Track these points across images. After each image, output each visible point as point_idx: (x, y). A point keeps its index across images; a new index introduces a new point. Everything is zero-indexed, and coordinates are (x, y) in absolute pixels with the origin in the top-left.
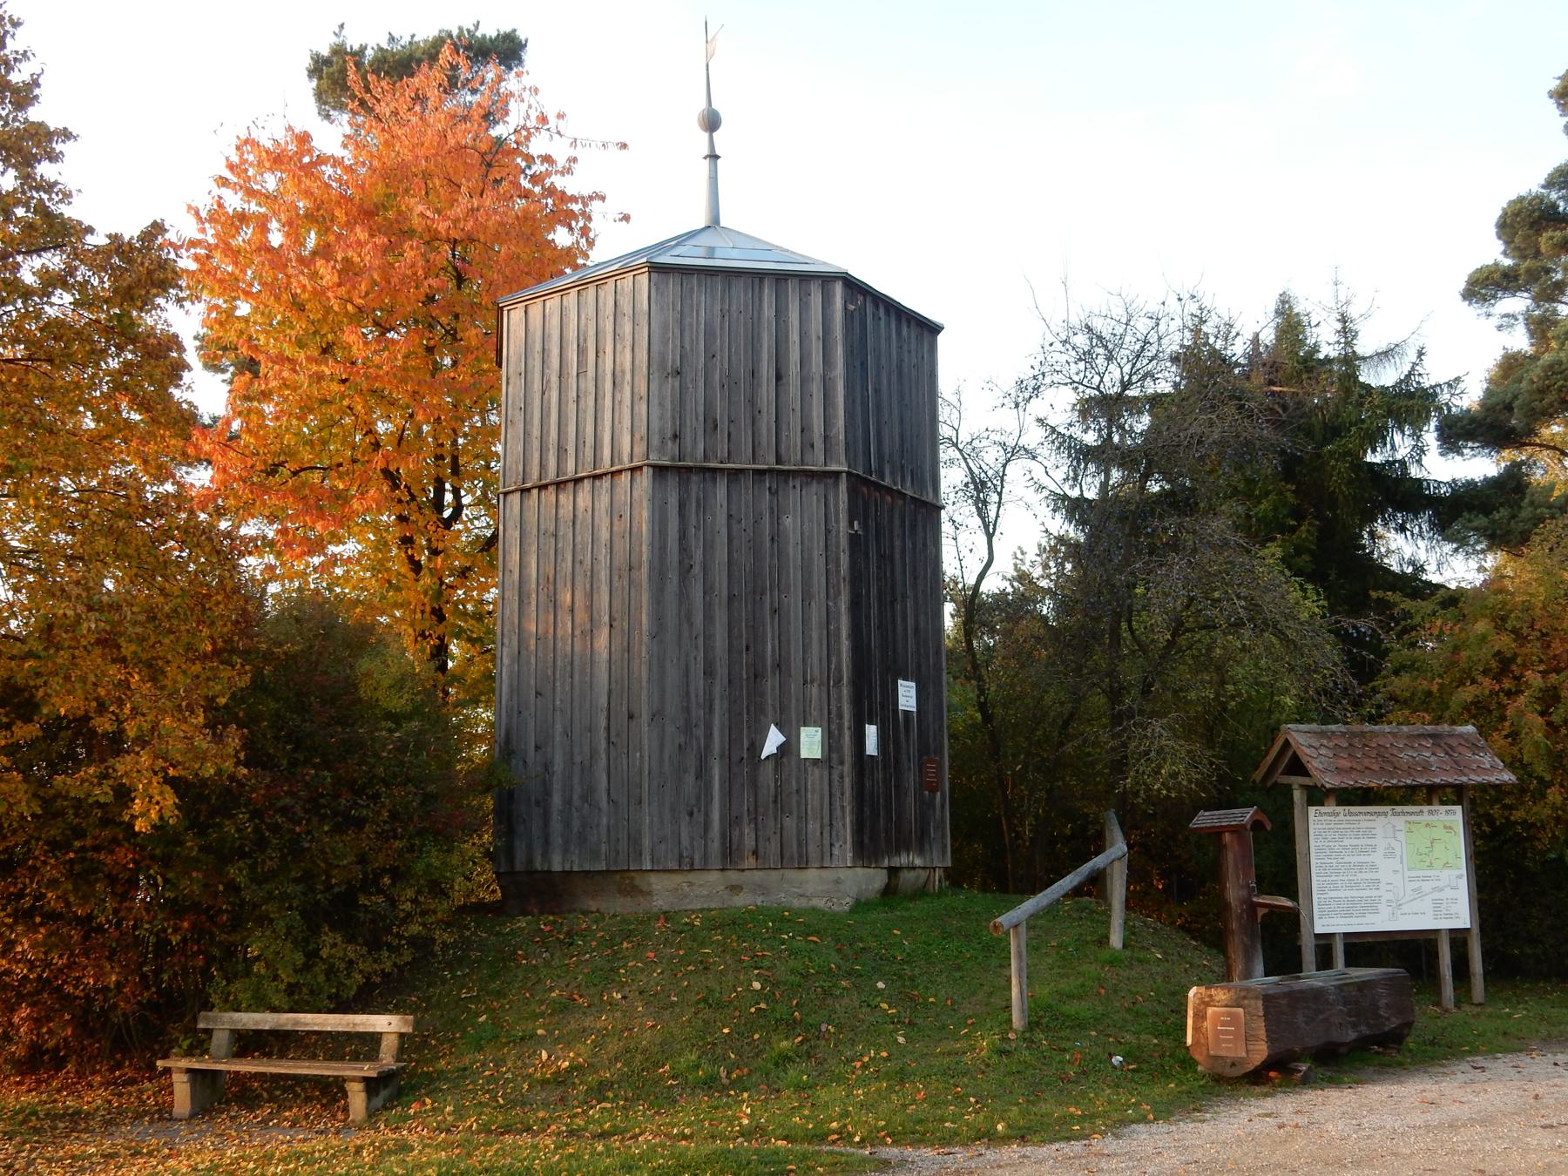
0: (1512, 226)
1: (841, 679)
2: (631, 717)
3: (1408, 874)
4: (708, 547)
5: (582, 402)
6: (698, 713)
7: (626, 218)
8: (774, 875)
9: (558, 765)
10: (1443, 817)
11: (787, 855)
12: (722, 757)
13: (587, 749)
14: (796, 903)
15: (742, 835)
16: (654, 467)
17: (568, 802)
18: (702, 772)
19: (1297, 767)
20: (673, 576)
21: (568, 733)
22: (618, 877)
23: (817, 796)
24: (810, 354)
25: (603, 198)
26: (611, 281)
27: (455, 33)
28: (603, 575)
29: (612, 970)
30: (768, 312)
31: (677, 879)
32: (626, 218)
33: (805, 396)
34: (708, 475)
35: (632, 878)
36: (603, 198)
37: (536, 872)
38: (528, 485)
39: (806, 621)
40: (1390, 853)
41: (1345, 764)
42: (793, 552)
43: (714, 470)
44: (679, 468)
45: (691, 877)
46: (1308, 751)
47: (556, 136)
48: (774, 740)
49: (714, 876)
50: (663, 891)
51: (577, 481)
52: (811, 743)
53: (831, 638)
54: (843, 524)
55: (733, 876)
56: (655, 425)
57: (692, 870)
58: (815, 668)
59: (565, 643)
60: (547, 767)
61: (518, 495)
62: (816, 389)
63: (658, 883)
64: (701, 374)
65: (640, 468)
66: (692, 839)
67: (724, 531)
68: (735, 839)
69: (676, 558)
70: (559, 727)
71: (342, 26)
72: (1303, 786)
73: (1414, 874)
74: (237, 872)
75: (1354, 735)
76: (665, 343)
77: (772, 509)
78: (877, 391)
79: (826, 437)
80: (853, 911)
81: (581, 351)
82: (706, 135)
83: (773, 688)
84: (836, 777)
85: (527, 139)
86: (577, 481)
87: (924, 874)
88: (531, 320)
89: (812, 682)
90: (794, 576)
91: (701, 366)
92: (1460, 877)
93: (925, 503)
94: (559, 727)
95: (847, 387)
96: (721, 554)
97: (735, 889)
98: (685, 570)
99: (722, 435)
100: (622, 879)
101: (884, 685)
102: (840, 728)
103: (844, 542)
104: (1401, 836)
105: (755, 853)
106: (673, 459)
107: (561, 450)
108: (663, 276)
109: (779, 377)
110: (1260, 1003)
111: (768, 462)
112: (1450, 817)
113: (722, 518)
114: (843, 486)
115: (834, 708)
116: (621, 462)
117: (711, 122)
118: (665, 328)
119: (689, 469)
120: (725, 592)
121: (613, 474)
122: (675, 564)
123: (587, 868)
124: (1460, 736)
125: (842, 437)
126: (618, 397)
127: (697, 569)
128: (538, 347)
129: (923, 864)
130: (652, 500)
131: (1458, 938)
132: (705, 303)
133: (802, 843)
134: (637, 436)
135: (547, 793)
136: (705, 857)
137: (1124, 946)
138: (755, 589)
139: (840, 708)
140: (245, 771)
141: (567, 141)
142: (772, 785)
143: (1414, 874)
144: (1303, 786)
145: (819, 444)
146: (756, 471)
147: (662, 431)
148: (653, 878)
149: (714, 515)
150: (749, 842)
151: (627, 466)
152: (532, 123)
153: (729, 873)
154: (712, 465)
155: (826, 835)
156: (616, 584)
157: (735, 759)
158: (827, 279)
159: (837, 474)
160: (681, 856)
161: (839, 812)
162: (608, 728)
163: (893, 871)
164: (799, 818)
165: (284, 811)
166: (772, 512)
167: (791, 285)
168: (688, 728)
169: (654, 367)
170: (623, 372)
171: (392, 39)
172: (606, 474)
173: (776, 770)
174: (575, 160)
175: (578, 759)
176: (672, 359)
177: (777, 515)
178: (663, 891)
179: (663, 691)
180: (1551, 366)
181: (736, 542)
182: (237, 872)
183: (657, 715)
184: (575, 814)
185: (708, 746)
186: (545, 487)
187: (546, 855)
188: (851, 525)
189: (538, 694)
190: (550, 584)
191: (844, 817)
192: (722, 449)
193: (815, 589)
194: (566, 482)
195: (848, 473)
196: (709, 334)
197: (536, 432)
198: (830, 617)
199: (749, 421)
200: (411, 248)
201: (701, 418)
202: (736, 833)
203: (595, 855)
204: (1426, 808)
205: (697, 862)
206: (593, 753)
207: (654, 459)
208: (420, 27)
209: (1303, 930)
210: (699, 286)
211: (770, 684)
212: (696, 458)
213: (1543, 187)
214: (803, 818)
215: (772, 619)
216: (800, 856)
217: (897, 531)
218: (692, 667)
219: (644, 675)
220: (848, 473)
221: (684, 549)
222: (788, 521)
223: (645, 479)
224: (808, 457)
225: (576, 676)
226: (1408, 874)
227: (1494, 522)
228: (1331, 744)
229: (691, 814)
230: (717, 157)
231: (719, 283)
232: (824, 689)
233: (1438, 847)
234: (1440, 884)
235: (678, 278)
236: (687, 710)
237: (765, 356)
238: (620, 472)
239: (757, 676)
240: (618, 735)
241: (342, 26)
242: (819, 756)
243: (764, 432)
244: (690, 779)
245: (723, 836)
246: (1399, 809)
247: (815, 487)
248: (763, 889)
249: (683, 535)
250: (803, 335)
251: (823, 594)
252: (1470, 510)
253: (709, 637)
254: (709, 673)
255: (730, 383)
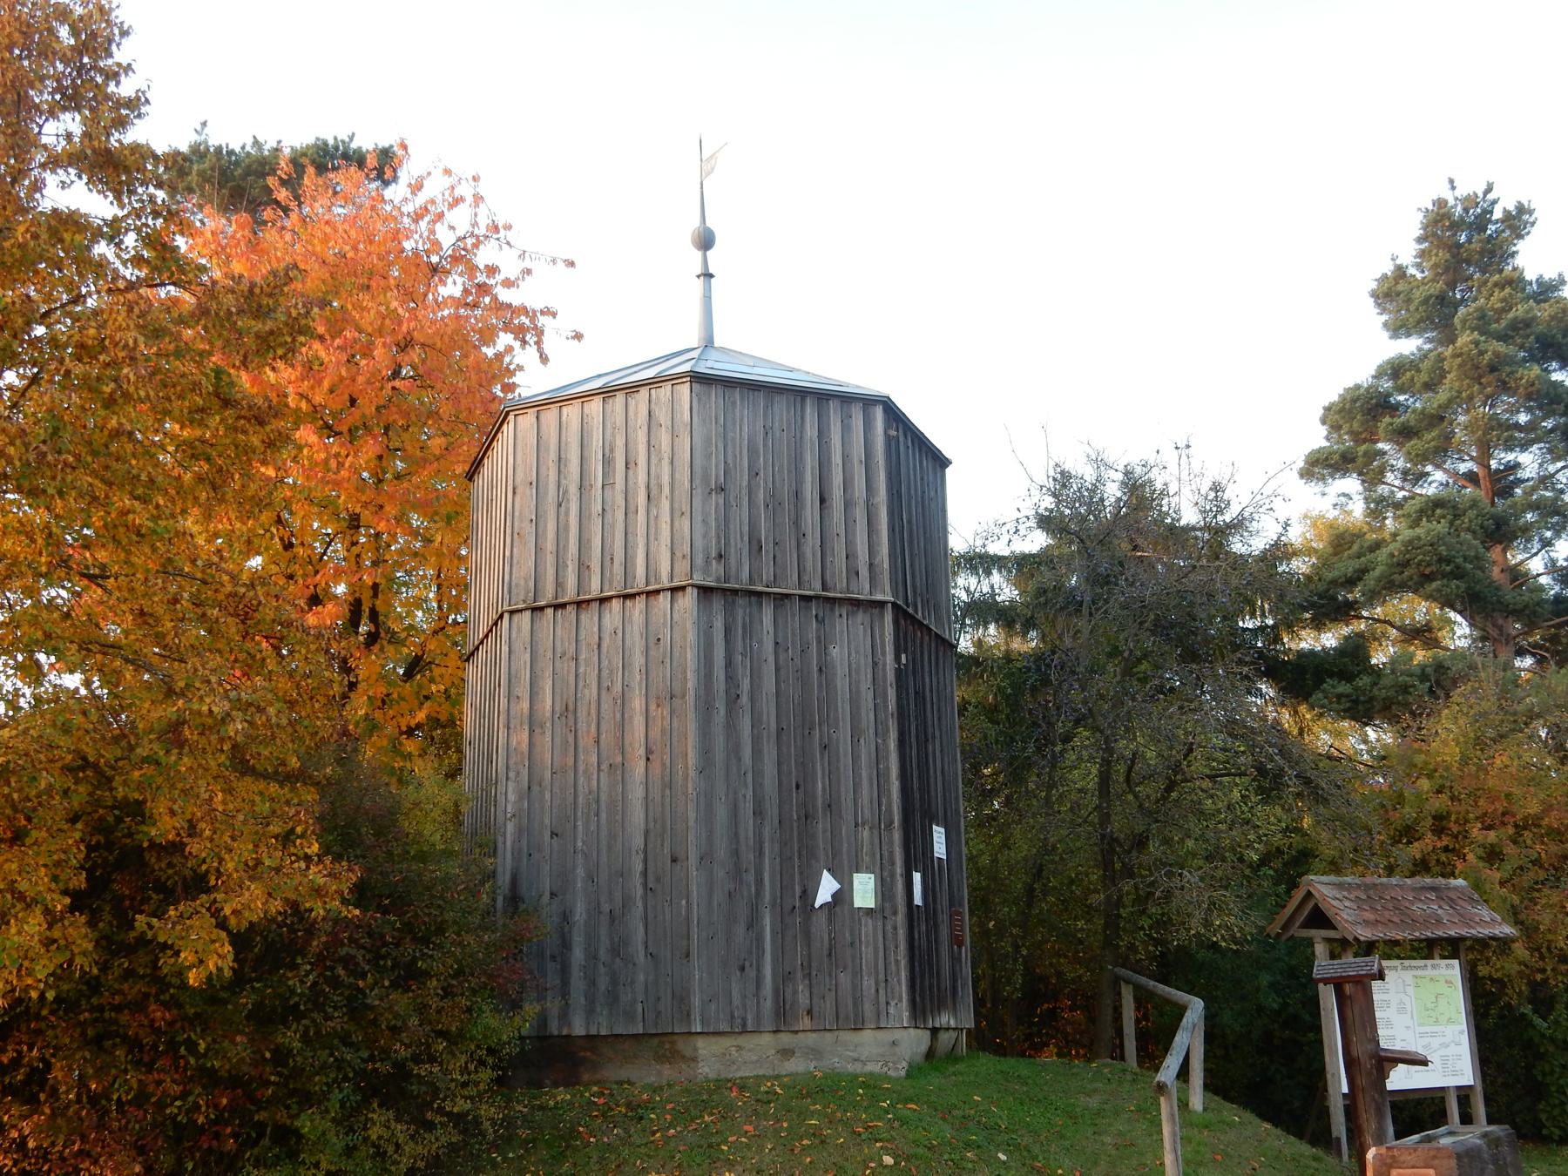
0: (1350, 411)
1: (892, 822)
2: (674, 860)
3: (1419, 1030)
4: (756, 675)
5: (609, 516)
6: (749, 857)
7: (578, 336)
8: (829, 1037)
9: (580, 913)
10: (1443, 971)
11: (842, 1016)
12: (773, 905)
13: (618, 895)
14: (850, 1068)
15: (795, 992)
16: (699, 587)
17: (592, 956)
18: (753, 923)
19: (1319, 919)
20: (720, 705)
21: (591, 878)
22: (656, 1041)
23: (871, 948)
24: (853, 478)
25: (554, 315)
26: (644, 392)
27: (331, 142)
28: (637, 704)
29: (710, 1146)
30: (811, 431)
31: (727, 1042)
32: (578, 336)
33: (849, 521)
34: (753, 599)
35: (673, 1043)
36: (554, 315)
37: (552, 1036)
38: (542, 603)
39: (856, 758)
40: (1402, 1010)
41: (1369, 916)
42: (842, 685)
43: (759, 594)
44: (724, 590)
45: (742, 1040)
46: (1335, 903)
47: (505, 247)
48: (827, 887)
49: (766, 1039)
50: (712, 1058)
51: (603, 600)
52: (864, 890)
53: (881, 777)
54: (890, 657)
55: (786, 1039)
56: (699, 543)
57: (744, 1032)
58: (866, 812)
59: (589, 779)
60: (566, 917)
61: (528, 613)
62: (860, 514)
63: (704, 1047)
64: (745, 491)
65: (683, 588)
66: (744, 997)
67: (771, 659)
68: (789, 997)
69: (722, 687)
70: (580, 872)
71: (204, 124)
72: (1328, 940)
73: (1423, 1029)
74: (290, 1038)
75: (1367, 887)
76: (708, 456)
77: (818, 638)
78: (909, 522)
79: (871, 565)
80: (909, 1076)
81: (608, 462)
82: (700, 254)
83: (824, 831)
84: (889, 928)
85: (476, 246)
86: (603, 600)
87: (954, 1035)
88: (544, 427)
89: (863, 824)
90: (844, 709)
91: (745, 483)
92: (1461, 1032)
93: (944, 640)
94: (580, 872)
95: (891, 514)
96: (769, 684)
97: (787, 1053)
98: (733, 700)
99: (766, 557)
100: (663, 1043)
101: (923, 831)
102: (892, 875)
103: (891, 676)
104: (1410, 990)
105: (809, 1012)
106: (718, 580)
107: (583, 567)
108: (704, 388)
109: (822, 501)
110: (1453, 1163)
111: (816, 589)
112: (1450, 972)
113: (769, 646)
114: (888, 617)
115: (886, 854)
116: (658, 581)
117: (705, 241)
118: (708, 441)
119: (735, 592)
120: (773, 725)
121: (648, 594)
122: (722, 694)
123: (619, 1030)
124: (1456, 888)
125: (886, 565)
126: (654, 512)
127: (745, 699)
128: (553, 455)
129: (957, 1020)
130: (698, 622)
131: (1464, 1094)
132: (748, 418)
133: (857, 1001)
134: (678, 554)
135: (566, 944)
136: (758, 1017)
137: (1205, 1109)
138: (804, 722)
139: (891, 853)
140: (357, 912)
141: (515, 253)
142: (826, 937)
143: (1423, 1029)
144: (1328, 940)
145: (864, 572)
146: (802, 598)
147: (706, 550)
148: (701, 1043)
149: (760, 642)
150: (803, 1000)
151: (668, 585)
152: (481, 231)
153: (782, 1035)
154: (759, 589)
155: (882, 992)
156: (652, 713)
157: (787, 908)
158: (869, 402)
159: (882, 604)
160: (733, 1017)
161: (893, 968)
162: (645, 873)
163: (935, 1031)
164: (854, 975)
165: (347, 961)
166: (819, 642)
167: (833, 405)
168: (737, 873)
169: (697, 482)
170: (660, 487)
171: (256, 142)
172: (639, 594)
173: (830, 920)
174: (529, 272)
175: (606, 908)
176: (716, 474)
177: (824, 644)
178: (712, 1058)
179: (711, 832)
180: (1410, 542)
181: (782, 672)
182: (290, 1038)
183: (706, 858)
184: (602, 970)
185: (759, 893)
186: (563, 606)
187: (564, 1016)
188: (897, 659)
189: (554, 834)
190: (568, 712)
191: (898, 973)
192: (768, 572)
193: (864, 724)
194: (588, 601)
195: (894, 604)
196: (753, 452)
197: (550, 545)
198: (880, 755)
199: (794, 543)
200: (384, 344)
201: (746, 538)
202: (789, 991)
203: (630, 1016)
204: (1429, 962)
205: (749, 1022)
206: (627, 902)
207: (698, 579)
208: (291, 132)
209: (1330, 1090)
210: (742, 399)
211: (821, 826)
212: (742, 580)
213: (1374, 377)
214: (857, 974)
215: (822, 754)
216: (856, 1015)
217: (927, 669)
218: (741, 805)
219: (692, 815)
220: (894, 604)
221: (730, 678)
222: (835, 652)
223: (688, 600)
224: (853, 586)
225: (604, 815)
226: (1419, 1030)
227: (1356, 689)
228: (1352, 896)
229: (742, 969)
230: (711, 276)
231: (761, 399)
232: (876, 833)
233: (1442, 1001)
234: (1446, 1040)
235: (720, 390)
236: (736, 853)
237: (808, 477)
238: (657, 592)
239: (807, 817)
240: (658, 880)
241: (204, 124)
242: (872, 906)
243: (809, 555)
244: (740, 930)
245: (776, 992)
246: (1407, 963)
247: (861, 617)
248: (816, 1053)
249: (729, 663)
250: (846, 458)
251: (872, 731)
252: (1331, 676)
253: (758, 774)
254: (758, 813)
255: (773, 504)
